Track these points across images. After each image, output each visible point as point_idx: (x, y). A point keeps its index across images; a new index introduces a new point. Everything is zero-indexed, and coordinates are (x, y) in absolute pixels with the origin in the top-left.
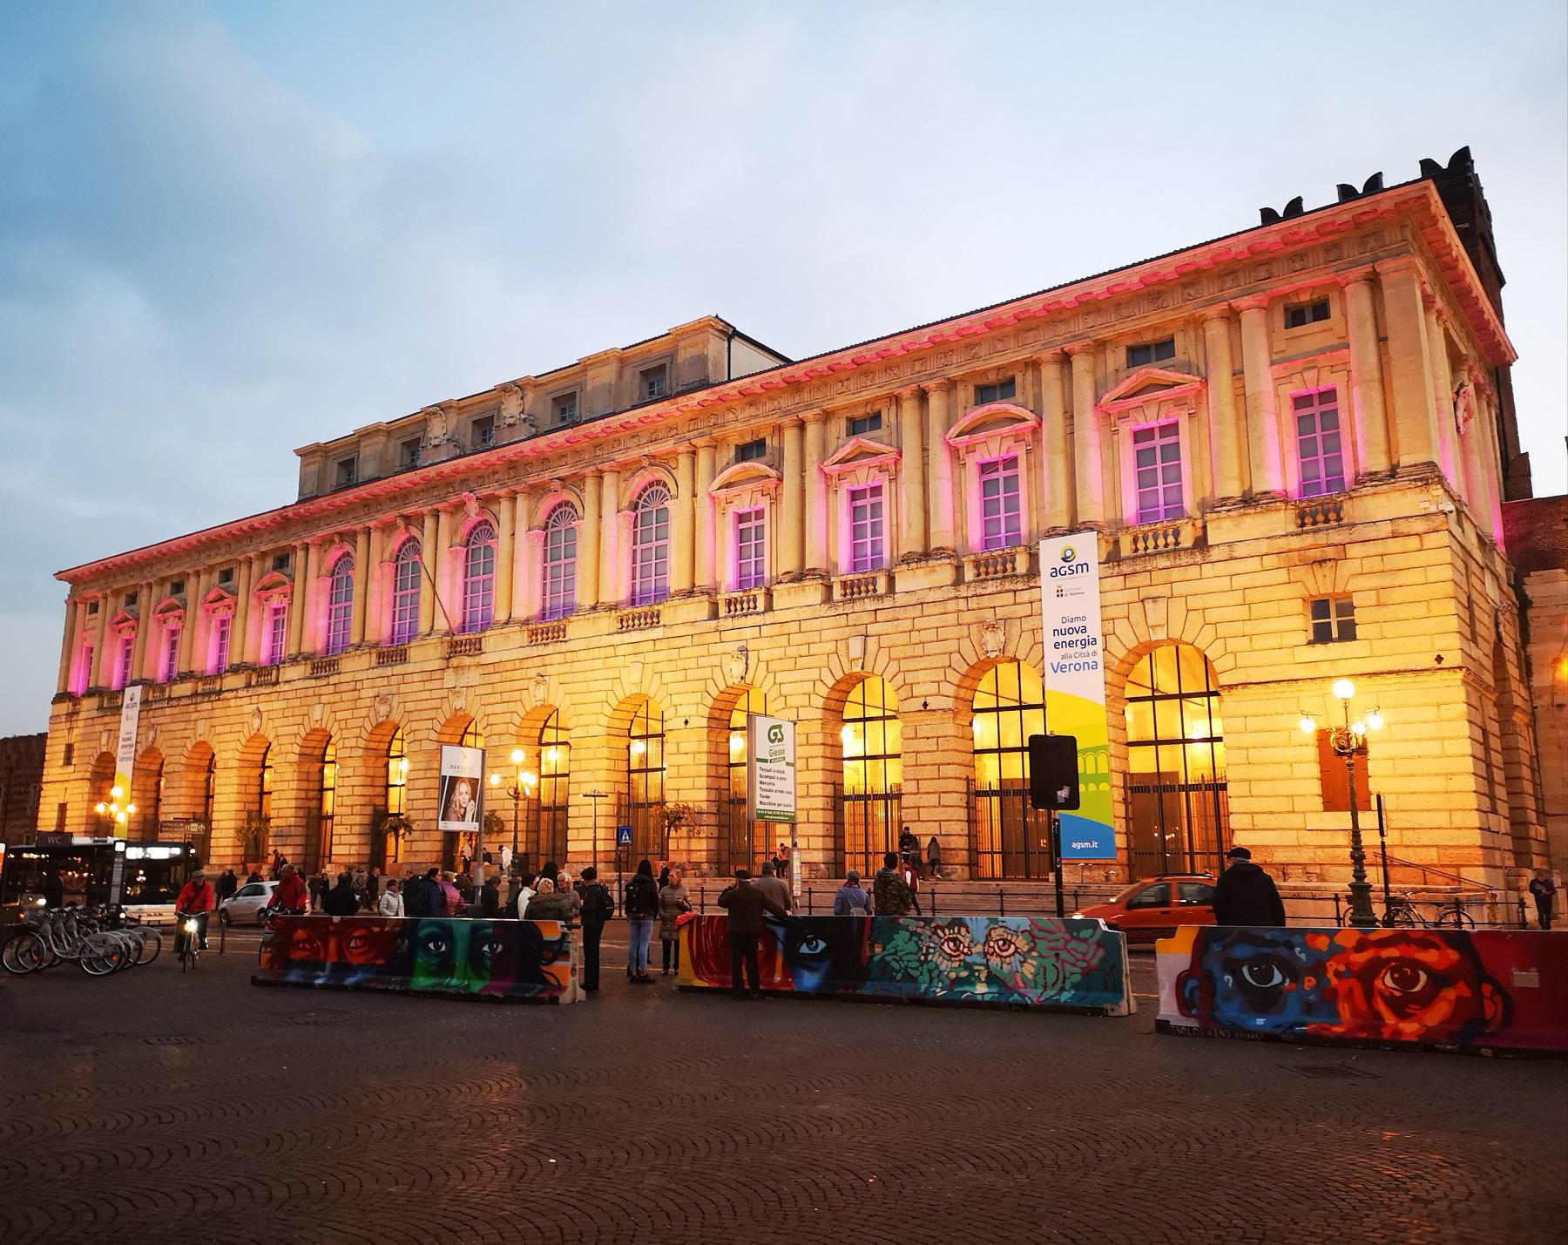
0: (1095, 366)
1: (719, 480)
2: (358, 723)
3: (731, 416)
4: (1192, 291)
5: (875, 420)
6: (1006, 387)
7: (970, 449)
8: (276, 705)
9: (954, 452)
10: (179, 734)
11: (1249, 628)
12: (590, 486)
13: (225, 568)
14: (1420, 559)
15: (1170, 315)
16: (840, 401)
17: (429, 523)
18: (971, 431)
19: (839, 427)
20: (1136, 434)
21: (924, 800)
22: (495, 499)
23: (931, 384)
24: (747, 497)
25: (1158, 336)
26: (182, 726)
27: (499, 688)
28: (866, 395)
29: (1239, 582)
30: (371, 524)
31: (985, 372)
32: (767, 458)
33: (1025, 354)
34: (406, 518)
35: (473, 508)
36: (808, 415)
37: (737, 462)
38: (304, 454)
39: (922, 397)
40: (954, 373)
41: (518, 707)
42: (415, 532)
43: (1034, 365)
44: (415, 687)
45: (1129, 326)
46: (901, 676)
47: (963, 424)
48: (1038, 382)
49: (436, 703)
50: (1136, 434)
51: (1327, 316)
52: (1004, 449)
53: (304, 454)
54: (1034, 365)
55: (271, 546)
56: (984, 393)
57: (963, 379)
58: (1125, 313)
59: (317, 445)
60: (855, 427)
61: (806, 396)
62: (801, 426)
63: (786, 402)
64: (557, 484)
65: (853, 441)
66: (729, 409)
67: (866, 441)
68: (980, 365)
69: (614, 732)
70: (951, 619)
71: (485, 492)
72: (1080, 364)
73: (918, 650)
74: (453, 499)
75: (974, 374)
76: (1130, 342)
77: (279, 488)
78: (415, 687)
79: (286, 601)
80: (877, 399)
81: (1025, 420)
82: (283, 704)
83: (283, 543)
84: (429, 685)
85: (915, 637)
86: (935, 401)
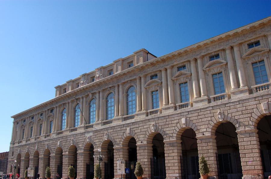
0: (240, 49)
1: (147, 84)
2: (67, 145)
3: (149, 69)
4: (263, 29)
5: (156, 75)
6: (217, 56)
7: (209, 71)
8: (51, 142)
9: (173, 81)
10: (32, 149)
12: (116, 88)
13: (32, 116)
14: (248, 104)
15: (258, 36)
16: (175, 63)
17: (81, 100)
18: (209, 67)
19: (175, 69)
20: (252, 64)
21: (172, 161)
22: (95, 93)
23: (198, 57)
24: (154, 87)
25: (255, 40)
26: (33, 147)
27: (97, 136)
28: (182, 61)
30: (70, 101)
31: (211, 53)
32: (158, 78)
33: (222, 48)
34: (77, 99)
35: (91, 95)
36: (167, 67)
37: (151, 80)
38: (56, 88)
39: (196, 60)
40: (203, 54)
41: (102, 140)
42: (78, 102)
43: (224, 50)
44: (79, 137)
45: (248, 39)
46: (196, 127)
47: (207, 65)
48: (225, 55)
49: (83, 140)
50: (252, 64)
51: (259, 45)
52: (218, 70)
53: (56, 88)
54: (224, 50)
55: (50, 108)
56: (212, 58)
57: (206, 55)
58: (246, 36)
59: (59, 86)
60: (179, 68)
61: (167, 63)
62: (166, 70)
63: (162, 65)
64: (109, 89)
65: (179, 72)
66: (148, 68)
67: (183, 71)
68: (210, 52)
69: (104, 148)
70: (209, 112)
71: (93, 92)
72: (236, 49)
74: (86, 94)
75: (209, 54)
76: (248, 43)
77: (51, 95)
78: (79, 137)
79: (53, 119)
80: (184, 62)
81: (223, 63)
82: (52, 142)
83: (52, 107)
84: (82, 136)
85: (199, 117)
86: (199, 61)
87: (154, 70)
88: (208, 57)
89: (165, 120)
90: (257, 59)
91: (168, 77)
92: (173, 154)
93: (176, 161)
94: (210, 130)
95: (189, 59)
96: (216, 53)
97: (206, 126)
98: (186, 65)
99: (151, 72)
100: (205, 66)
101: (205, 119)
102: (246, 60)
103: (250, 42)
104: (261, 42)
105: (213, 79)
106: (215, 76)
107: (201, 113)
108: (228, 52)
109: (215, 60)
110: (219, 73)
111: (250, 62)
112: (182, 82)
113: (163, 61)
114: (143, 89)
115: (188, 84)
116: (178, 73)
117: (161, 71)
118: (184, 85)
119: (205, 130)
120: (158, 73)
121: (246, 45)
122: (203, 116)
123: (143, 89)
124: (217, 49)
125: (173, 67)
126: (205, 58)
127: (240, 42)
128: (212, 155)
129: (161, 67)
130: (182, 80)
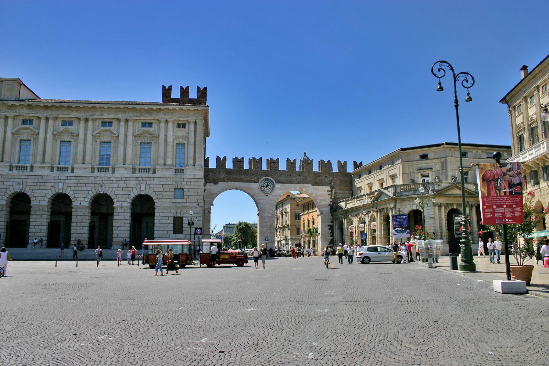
6: (71, 123)
11: (163, 193)
16: (61, 116)
29: (162, 183)
33: (117, 117)
45: (143, 118)
68: (104, 117)
72: (130, 124)
73: (80, 188)
76: (142, 121)
85: (79, 185)
87: (30, 115)
88: (100, 121)
89: (36, 181)
90: (146, 140)
91: (49, 130)
92: (42, 220)
93: (45, 227)
94: (88, 200)
95: (40, 115)
96: (109, 120)
97: (85, 196)
98: (34, 121)
99: (24, 114)
100: (96, 132)
101: (85, 189)
102: (57, 137)
103: (104, 120)
104: (153, 125)
105: (100, 147)
106: (103, 145)
107: (82, 181)
108: (122, 124)
109: (27, 126)
110: (28, 141)
111: (139, 142)
112: (25, 139)
113: (46, 107)
114: (89, 137)
115: (73, 144)
116: (62, 128)
117: (39, 118)
118: (26, 143)
119: (83, 199)
120: (34, 119)
121: (140, 123)
122: (84, 185)
123: (89, 137)
124: (112, 117)
125: (56, 118)
126: (97, 121)
127: (136, 118)
128: (45, 220)
129: (43, 114)
130: (66, 138)
